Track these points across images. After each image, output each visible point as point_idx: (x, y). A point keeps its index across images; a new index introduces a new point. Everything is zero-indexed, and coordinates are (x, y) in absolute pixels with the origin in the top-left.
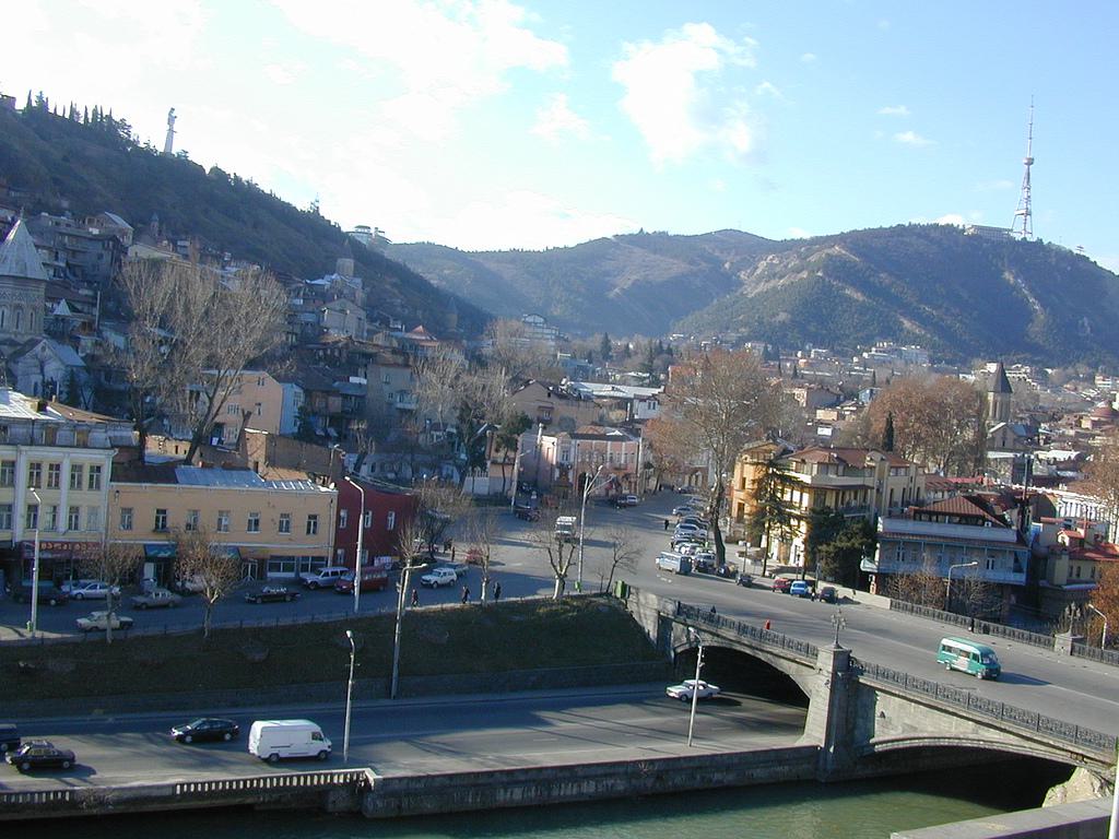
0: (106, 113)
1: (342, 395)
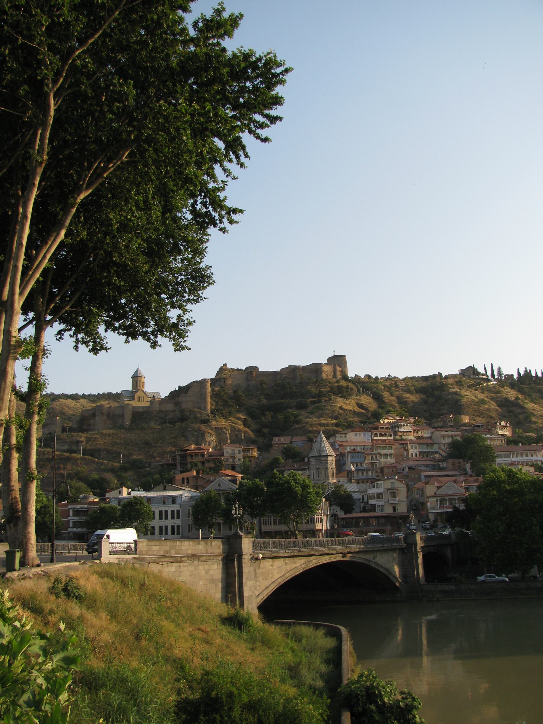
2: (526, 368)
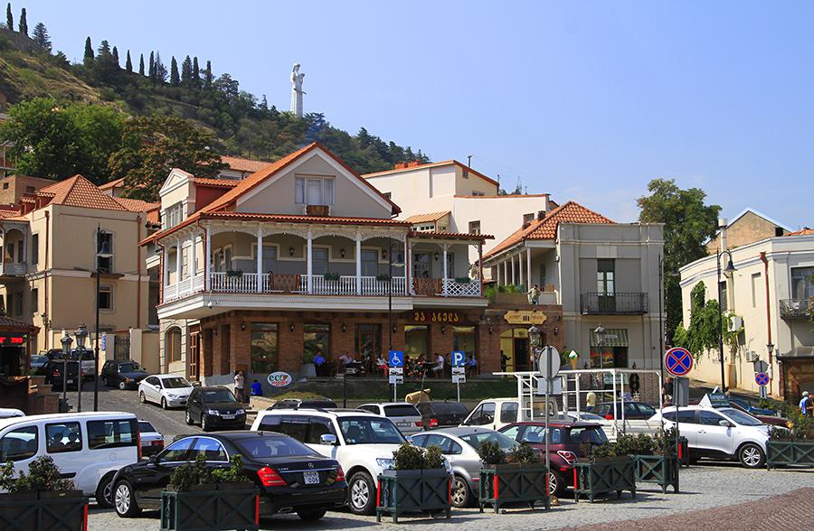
0: (202, 66)
2: (105, 43)
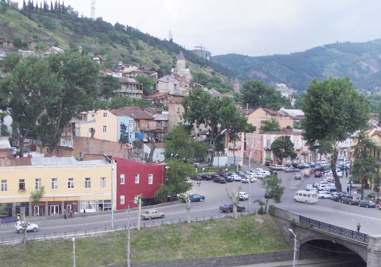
0: (61, 4)
1: (156, 121)
